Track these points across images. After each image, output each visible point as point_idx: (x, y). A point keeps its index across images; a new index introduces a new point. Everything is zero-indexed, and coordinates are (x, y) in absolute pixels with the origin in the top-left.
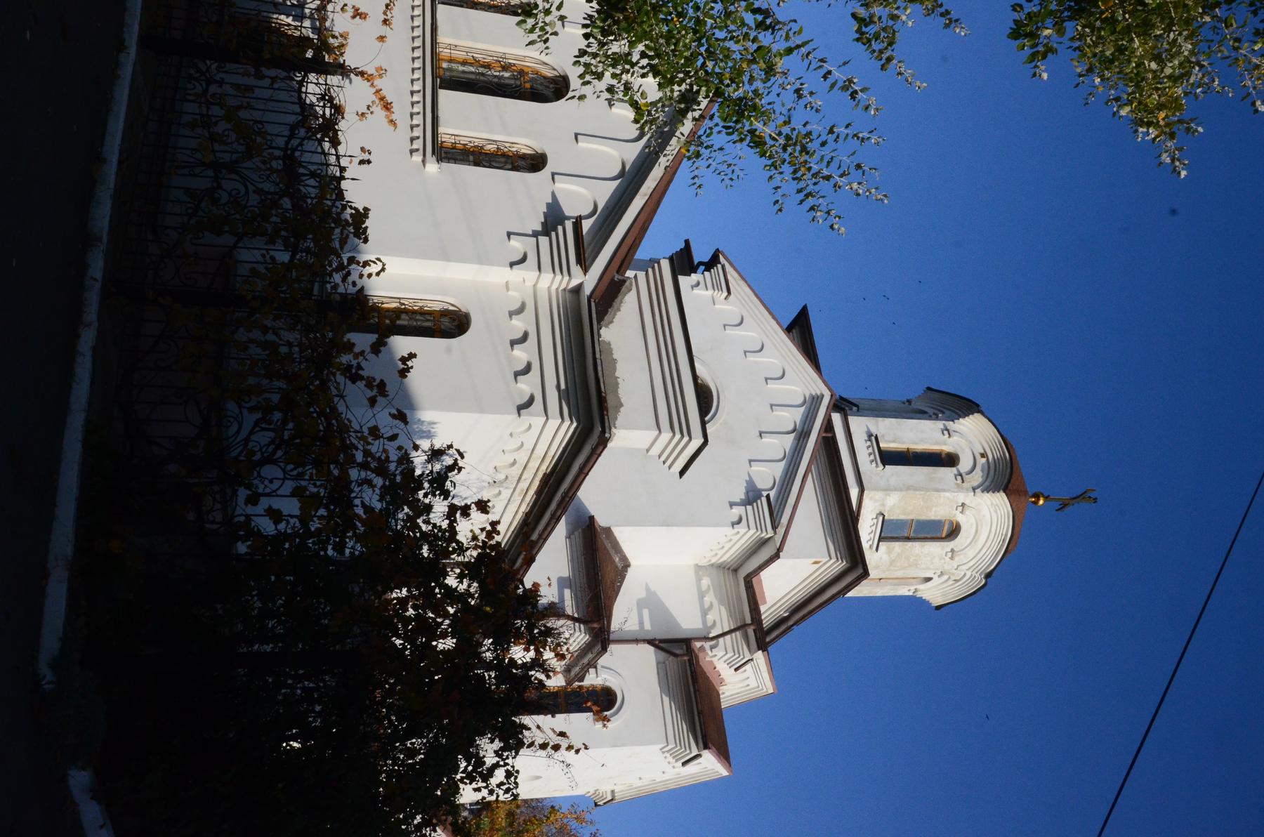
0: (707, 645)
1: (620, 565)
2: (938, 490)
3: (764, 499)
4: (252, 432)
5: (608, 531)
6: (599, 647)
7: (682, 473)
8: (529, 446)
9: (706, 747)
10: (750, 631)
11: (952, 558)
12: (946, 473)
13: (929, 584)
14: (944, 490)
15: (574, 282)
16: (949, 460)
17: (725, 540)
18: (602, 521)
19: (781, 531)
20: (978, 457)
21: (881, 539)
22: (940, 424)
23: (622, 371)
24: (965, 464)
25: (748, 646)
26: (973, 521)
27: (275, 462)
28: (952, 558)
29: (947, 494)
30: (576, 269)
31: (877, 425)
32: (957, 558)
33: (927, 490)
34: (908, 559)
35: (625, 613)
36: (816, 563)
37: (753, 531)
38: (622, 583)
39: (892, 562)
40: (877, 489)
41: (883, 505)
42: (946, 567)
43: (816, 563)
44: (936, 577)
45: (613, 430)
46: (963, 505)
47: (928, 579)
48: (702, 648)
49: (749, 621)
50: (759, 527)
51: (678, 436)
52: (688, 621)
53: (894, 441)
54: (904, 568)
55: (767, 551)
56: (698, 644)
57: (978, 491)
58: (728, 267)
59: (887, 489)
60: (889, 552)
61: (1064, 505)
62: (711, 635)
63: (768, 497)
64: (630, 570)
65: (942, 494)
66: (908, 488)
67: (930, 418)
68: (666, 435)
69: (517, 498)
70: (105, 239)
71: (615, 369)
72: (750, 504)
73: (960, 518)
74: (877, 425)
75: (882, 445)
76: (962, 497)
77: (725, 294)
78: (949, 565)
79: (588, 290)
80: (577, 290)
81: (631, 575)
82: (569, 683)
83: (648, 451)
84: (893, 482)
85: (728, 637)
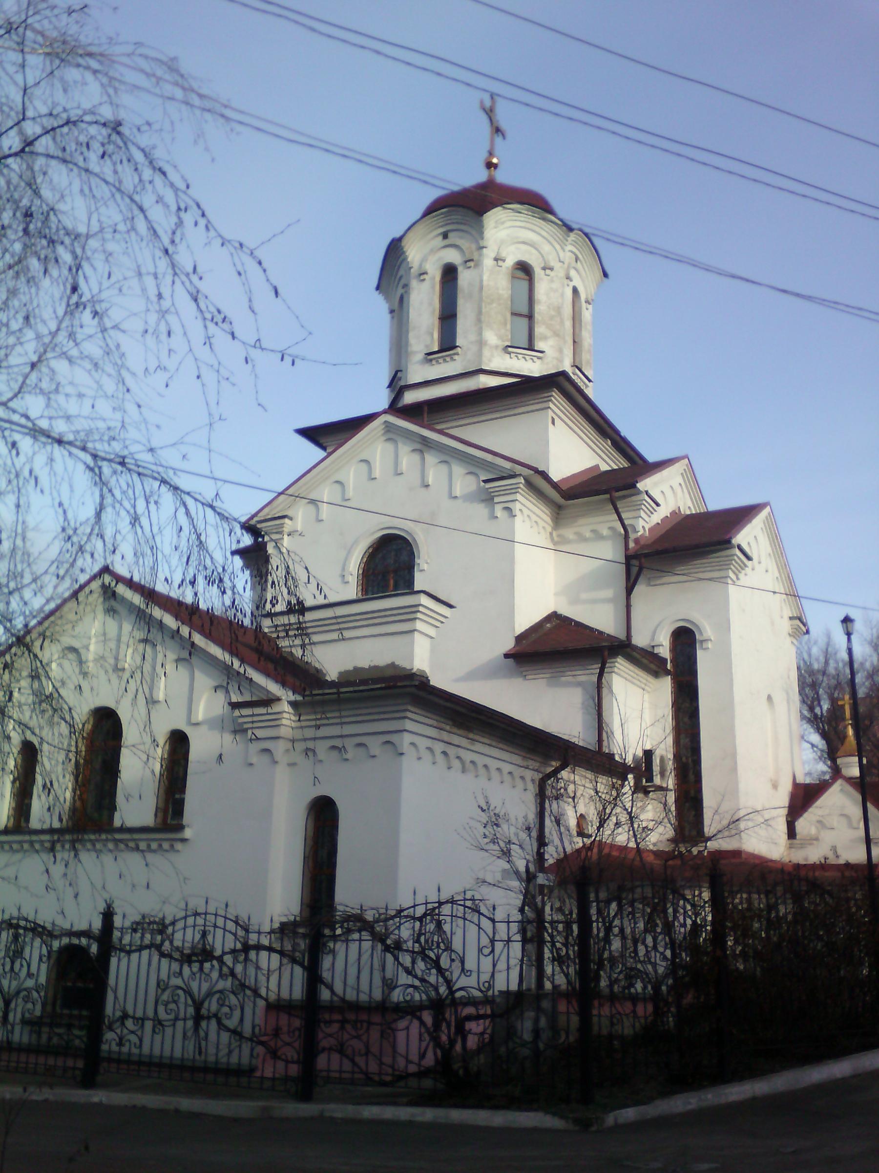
0: (632, 536)
1: (555, 622)
2: (481, 288)
3: (488, 485)
4: (416, 976)
5: (519, 639)
6: (628, 650)
7: (451, 606)
8: (428, 743)
9: (728, 542)
10: (617, 494)
11: (551, 269)
12: (465, 277)
13: (581, 289)
14: (481, 281)
15: (287, 708)
16: (450, 273)
17: (529, 520)
18: (509, 644)
19: (518, 469)
20: (447, 242)
21: (531, 348)
22: (414, 283)
23: (364, 663)
24: (453, 256)
25: (633, 495)
26: (512, 248)
27: (438, 957)
28: (551, 269)
29: (485, 278)
30: (276, 708)
31: (416, 352)
32: (552, 264)
33: (481, 300)
34: (552, 318)
35: (602, 618)
36: (553, 423)
37: (518, 497)
38: (572, 620)
39: (556, 334)
40: (480, 354)
41: (497, 347)
42: (562, 274)
43: (553, 423)
44: (572, 284)
45: (414, 670)
46: (496, 259)
47: (575, 291)
48: (636, 541)
49: (608, 496)
50: (514, 490)
51: (419, 615)
52: (609, 551)
53: (432, 335)
54: (562, 322)
55: (538, 482)
56: (632, 545)
57: (482, 244)
58: (256, 519)
59: (481, 343)
60: (545, 338)
61: (498, 130)
62: (622, 531)
63: (485, 481)
64: (560, 612)
65: (485, 283)
66: (479, 320)
67: (407, 292)
68: (419, 625)
69: (478, 747)
70: (261, 1103)
71: (363, 669)
72: (492, 499)
73: (510, 262)
74: (416, 352)
75: (436, 349)
76: (488, 262)
77: (287, 521)
78: (559, 271)
79: (292, 697)
80: (294, 704)
81: (566, 610)
82: (668, 673)
83: (432, 638)
84: (472, 337)
85: (624, 516)
